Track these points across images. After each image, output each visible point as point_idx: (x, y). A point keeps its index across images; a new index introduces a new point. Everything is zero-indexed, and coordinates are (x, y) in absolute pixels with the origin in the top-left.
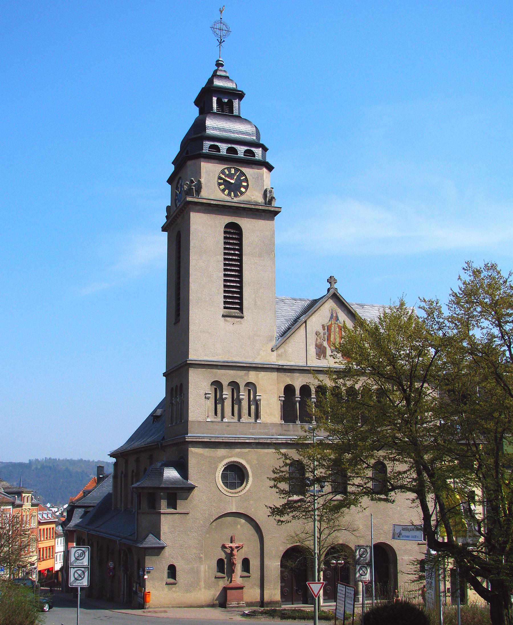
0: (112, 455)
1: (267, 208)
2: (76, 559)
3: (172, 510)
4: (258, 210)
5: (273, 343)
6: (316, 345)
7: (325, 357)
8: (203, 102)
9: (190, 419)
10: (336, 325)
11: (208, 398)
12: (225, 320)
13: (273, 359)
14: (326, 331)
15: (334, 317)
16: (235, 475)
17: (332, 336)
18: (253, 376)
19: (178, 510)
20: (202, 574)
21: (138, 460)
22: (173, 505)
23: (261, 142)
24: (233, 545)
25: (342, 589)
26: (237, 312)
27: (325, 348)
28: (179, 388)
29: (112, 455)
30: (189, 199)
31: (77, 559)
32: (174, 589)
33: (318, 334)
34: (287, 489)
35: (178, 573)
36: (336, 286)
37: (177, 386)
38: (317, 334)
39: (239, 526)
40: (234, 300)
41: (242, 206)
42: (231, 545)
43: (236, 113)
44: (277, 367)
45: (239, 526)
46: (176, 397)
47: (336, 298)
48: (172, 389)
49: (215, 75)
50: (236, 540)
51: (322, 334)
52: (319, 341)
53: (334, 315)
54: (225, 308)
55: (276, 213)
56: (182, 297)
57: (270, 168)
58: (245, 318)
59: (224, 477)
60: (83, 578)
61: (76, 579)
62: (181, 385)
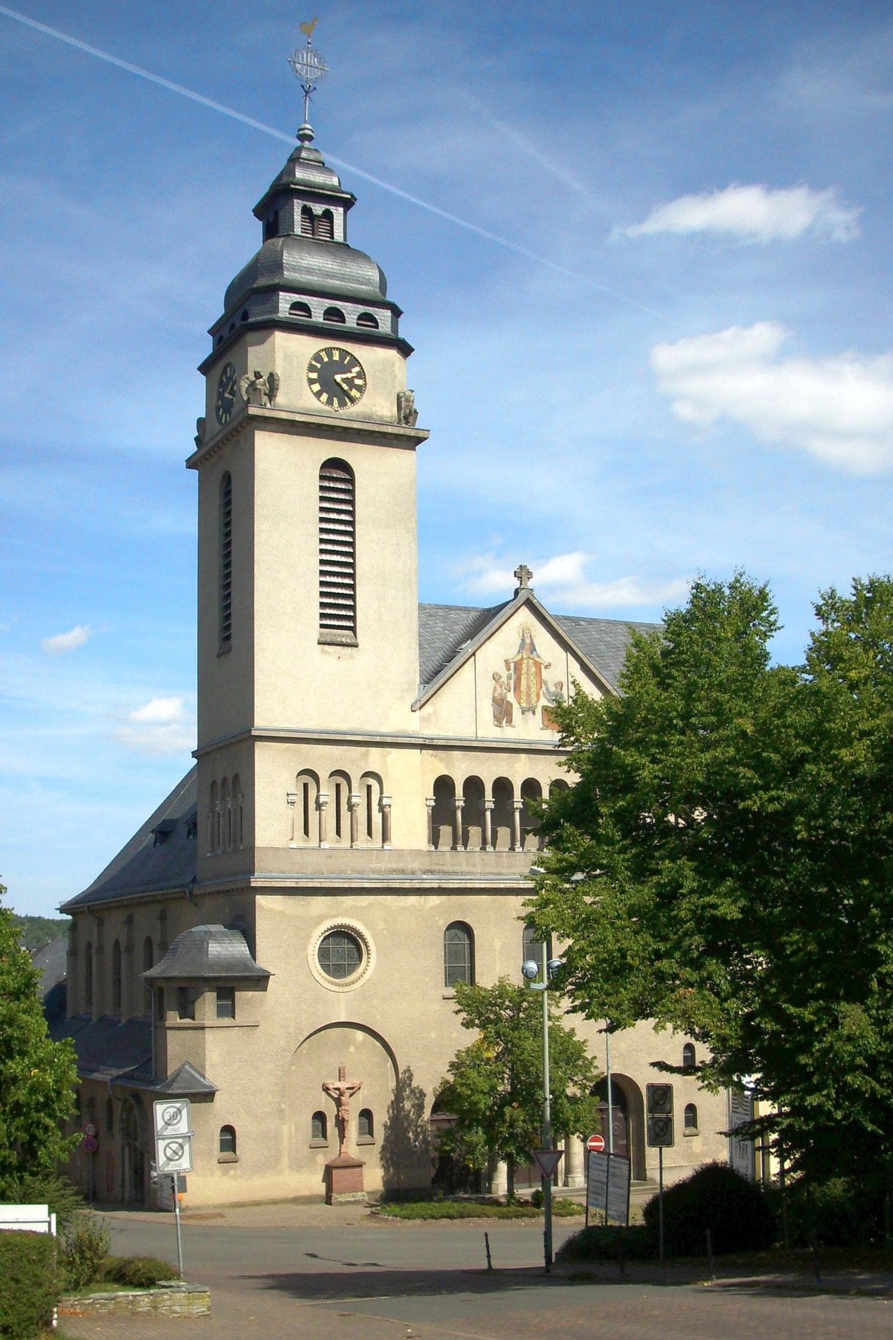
0: (62, 910)
1: (401, 431)
2: (166, 1123)
3: (227, 1021)
4: (384, 435)
5: (413, 696)
6: (494, 700)
7: (510, 722)
8: (272, 212)
9: (259, 843)
10: (531, 661)
11: (293, 803)
12: (322, 650)
13: (403, 721)
14: (512, 672)
15: (528, 646)
16: (343, 950)
17: (524, 682)
18: (375, 759)
19: (239, 1019)
20: (285, 1142)
21: (130, 921)
22: (227, 1009)
23: (389, 298)
24: (343, 1085)
25: (600, 1162)
26: (345, 636)
27: (511, 705)
28: (230, 783)
29: (62, 910)
30: (253, 411)
31: (168, 1124)
32: (232, 1172)
33: (497, 678)
34: (486, 980)
35: (238, 1142)
36: (531, 584)
37: (225, 779)
38: (496, 677)
39: (352, 1049)
40: (339, 612)
41: (355, 425)
42: (338, 1085)
43: (338, 236)
44: (421, 741)
45: (352, 1049)
46: (223, 799)
47: (530, 604)
48: (214, 784)
49: (294, 160)
50: (347, 1075)
51: (504, 679)
52: (499, 691)
53: (528, 641)
54: (322, 626)
55: (419, 440)
56: (235, 600)
57: (405, 350)
58: (360, 646)
59: (323, 954)
60: (180, 1157)
61: (170, 1159)
62: (236, 776)
